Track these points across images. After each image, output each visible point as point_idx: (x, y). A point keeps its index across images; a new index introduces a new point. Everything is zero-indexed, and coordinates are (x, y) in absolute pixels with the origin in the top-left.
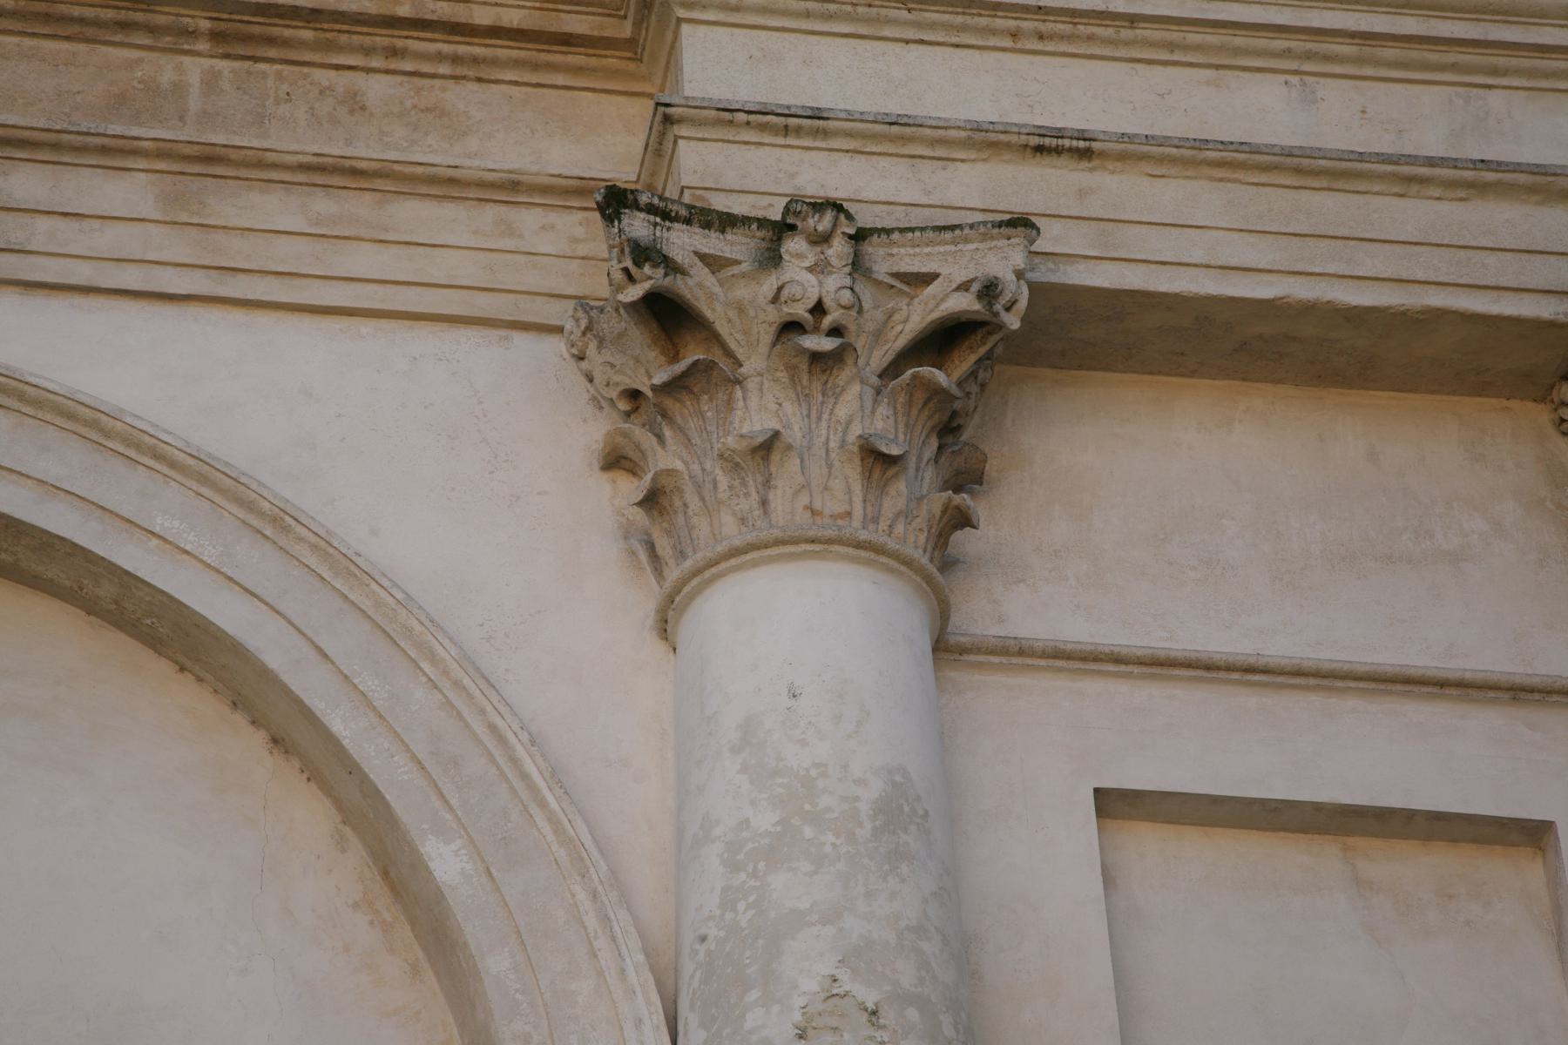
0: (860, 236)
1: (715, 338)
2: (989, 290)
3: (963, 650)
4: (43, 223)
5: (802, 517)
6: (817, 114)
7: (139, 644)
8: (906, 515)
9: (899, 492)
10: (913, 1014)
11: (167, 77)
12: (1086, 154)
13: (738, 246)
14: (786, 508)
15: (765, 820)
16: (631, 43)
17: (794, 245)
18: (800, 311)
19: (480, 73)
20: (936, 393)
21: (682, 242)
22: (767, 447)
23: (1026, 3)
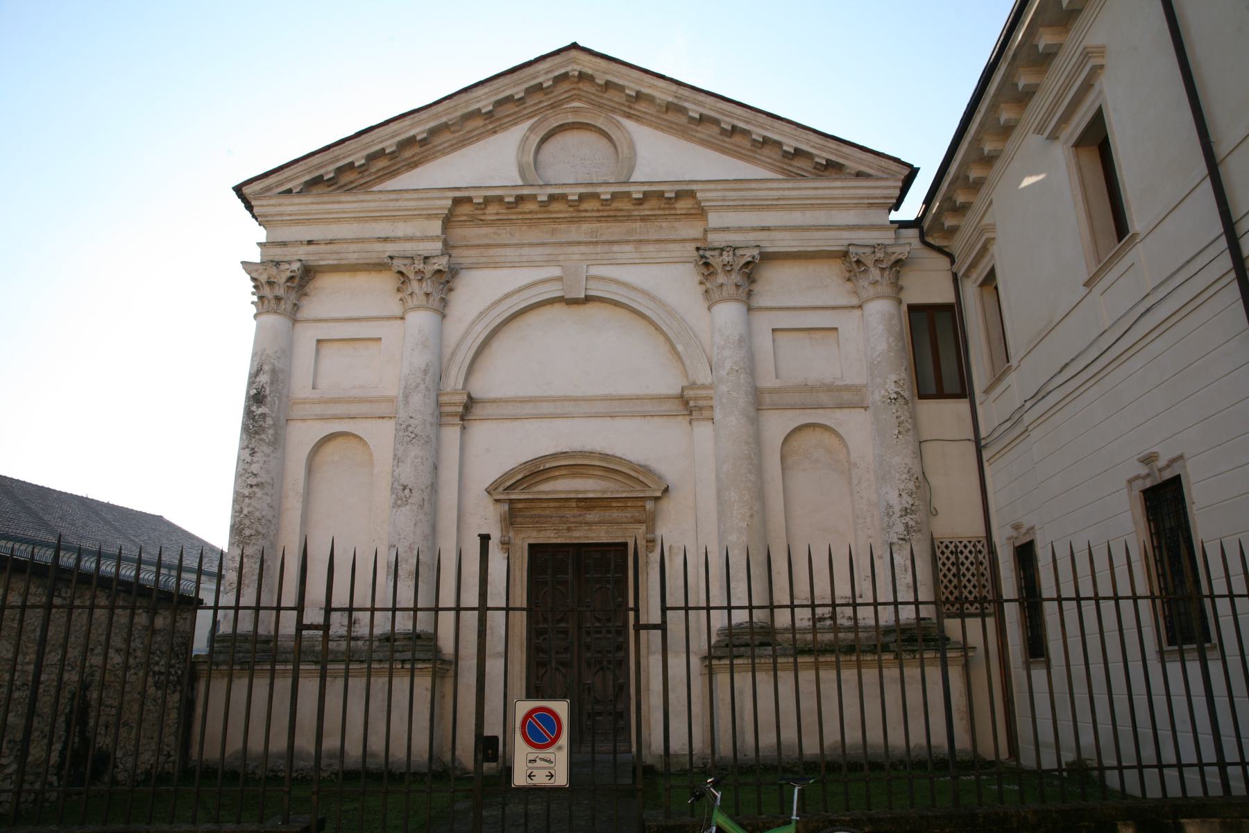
0: (735, 249)
1: (713, 267)
2: (753, 257)
3: (752, 309)
4: (619, 254)
5: (727, 295)
6: (728, 228)
8: (742, 292)
9: (741, 289)
10: (743, 370)
11: (634, 227)
12: (769, 230)
13: (716, 253)
14: (725, 294)
15: (722, 343)
16: (702, 214)
17: (724, 253)
18: (726, 263)
19: (679, 220)
20: (746, 273)
21: (708, 254)
22: (721, 285)
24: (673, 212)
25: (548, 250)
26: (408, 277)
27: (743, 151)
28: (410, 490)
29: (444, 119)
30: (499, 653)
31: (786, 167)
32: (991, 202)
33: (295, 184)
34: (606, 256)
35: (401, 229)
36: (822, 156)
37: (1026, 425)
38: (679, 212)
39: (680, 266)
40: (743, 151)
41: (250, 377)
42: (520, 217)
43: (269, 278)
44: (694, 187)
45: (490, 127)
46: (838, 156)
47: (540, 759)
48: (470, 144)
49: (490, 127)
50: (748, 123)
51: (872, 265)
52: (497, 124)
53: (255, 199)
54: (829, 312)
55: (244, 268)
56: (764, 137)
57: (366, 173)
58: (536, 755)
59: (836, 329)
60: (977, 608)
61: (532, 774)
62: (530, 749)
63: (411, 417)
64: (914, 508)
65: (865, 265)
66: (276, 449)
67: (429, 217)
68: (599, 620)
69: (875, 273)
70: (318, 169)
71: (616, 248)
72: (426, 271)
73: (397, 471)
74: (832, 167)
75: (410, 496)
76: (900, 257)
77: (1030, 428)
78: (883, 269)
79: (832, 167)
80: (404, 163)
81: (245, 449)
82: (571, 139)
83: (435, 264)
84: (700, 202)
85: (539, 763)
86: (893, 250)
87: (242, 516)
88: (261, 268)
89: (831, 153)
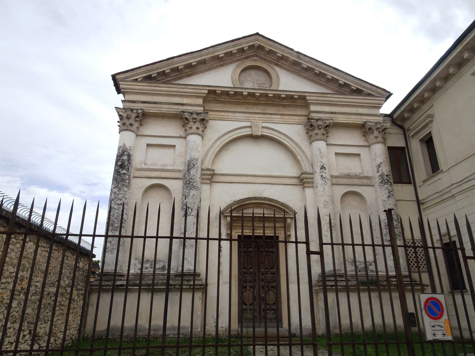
7: (438, 161)
23: (306, 252)
24: (296, 104)
25: (246, 115)
26: (189, 120)
27: (322, 82)
28: (192, 209)
29: (204, 58)
30: (226, 282)
31: (339, 90)
32: (433, 105)
33: (139, 77)
34: (269, 119)
35: (185, 101)
36: (354, 86)
37: (453, 194)
38: (298, 104)
39: (298, 126)
40: (322, 82)
41: (117, 156)
42: (234, 100)
43: (127, 115)
44: (306, 94)
45: (222, 63)
46: (361, 86)
47: (437, 325)
48: (212, 69)
49: (222, 63)
50: (326, 71)
51: (375, 130)
52: (224, 62)
53: (121, 81)
54: (357, 148)
55: (116, 110)
56: (332, 77)
57: (169, 76)
58: (435, 323)
59: (359, 155)
60: (426, 269)
61: (435, 334)
62: (432, 320)
63: (191, 179)
64: (397, 226)
65: (372, 130)
66: (129, 189)
67: (197, 97)
68: (267, 269)
69: (376, 133)
70: (149, 72)
71: (273, 116)
72: (197, 118)
73: (185, 201)
74: (358, 92)
75: (191, 212)
76: (386, 127)
77: (455, 195)
78: (380, 132)
79: (358, 92)
80: (185, 74)
81: (115, 188)
82: (253, 73)
83: (201, 116)
84: (308, 100)
85: (437, 328)
86: (383, 124)
87: (114, 218)
88: (124, 111)
89: (358, 85)
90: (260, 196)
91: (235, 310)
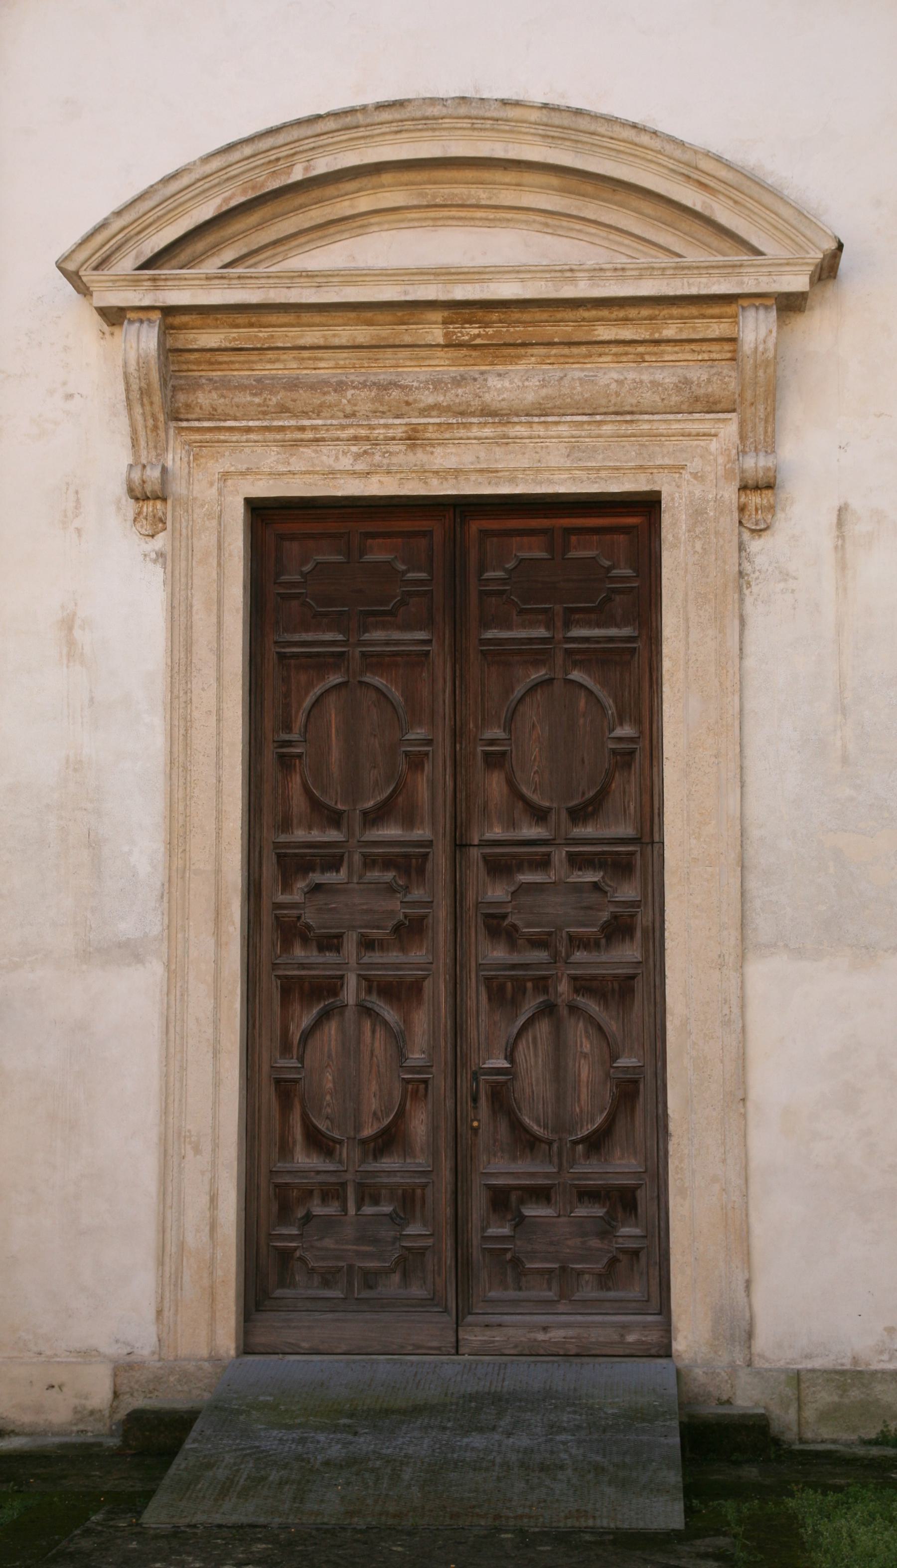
90: (477, 92)
91: (213, 1200)
